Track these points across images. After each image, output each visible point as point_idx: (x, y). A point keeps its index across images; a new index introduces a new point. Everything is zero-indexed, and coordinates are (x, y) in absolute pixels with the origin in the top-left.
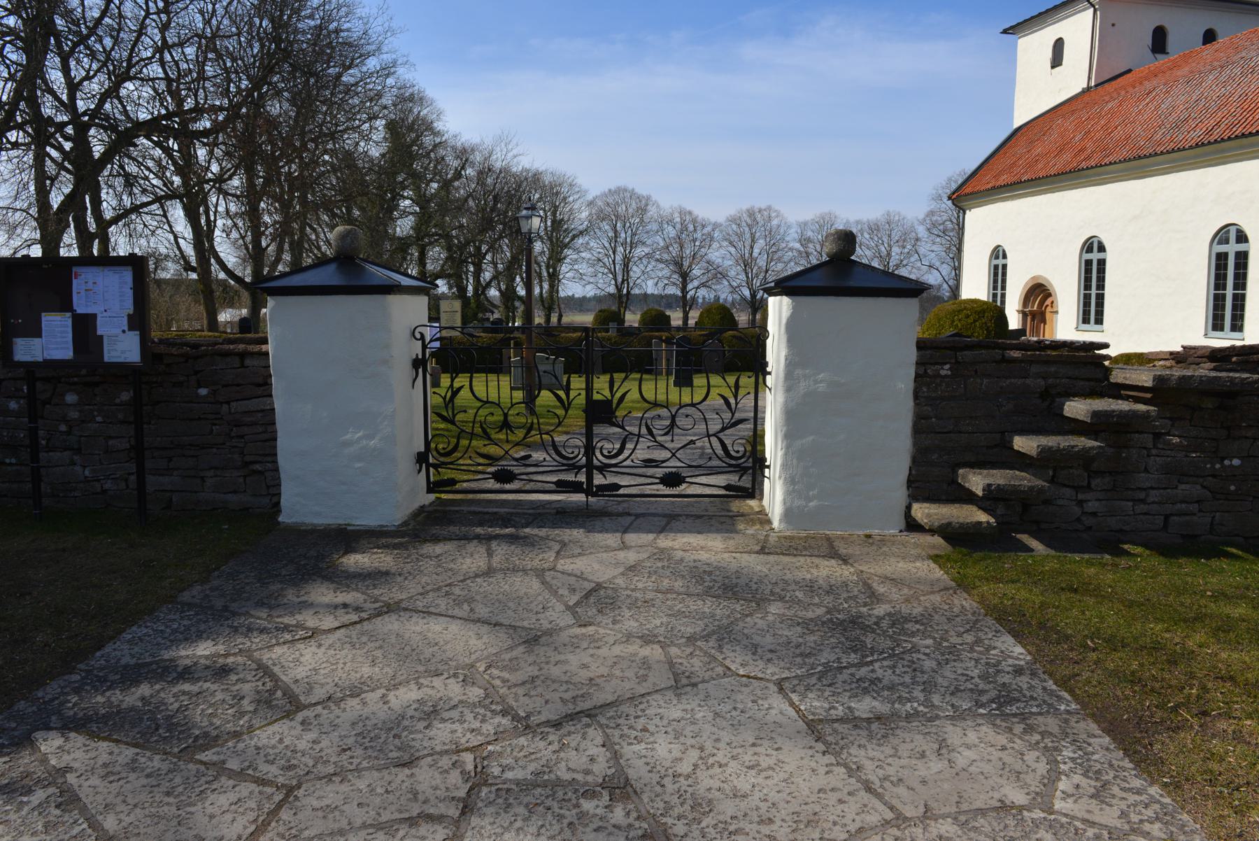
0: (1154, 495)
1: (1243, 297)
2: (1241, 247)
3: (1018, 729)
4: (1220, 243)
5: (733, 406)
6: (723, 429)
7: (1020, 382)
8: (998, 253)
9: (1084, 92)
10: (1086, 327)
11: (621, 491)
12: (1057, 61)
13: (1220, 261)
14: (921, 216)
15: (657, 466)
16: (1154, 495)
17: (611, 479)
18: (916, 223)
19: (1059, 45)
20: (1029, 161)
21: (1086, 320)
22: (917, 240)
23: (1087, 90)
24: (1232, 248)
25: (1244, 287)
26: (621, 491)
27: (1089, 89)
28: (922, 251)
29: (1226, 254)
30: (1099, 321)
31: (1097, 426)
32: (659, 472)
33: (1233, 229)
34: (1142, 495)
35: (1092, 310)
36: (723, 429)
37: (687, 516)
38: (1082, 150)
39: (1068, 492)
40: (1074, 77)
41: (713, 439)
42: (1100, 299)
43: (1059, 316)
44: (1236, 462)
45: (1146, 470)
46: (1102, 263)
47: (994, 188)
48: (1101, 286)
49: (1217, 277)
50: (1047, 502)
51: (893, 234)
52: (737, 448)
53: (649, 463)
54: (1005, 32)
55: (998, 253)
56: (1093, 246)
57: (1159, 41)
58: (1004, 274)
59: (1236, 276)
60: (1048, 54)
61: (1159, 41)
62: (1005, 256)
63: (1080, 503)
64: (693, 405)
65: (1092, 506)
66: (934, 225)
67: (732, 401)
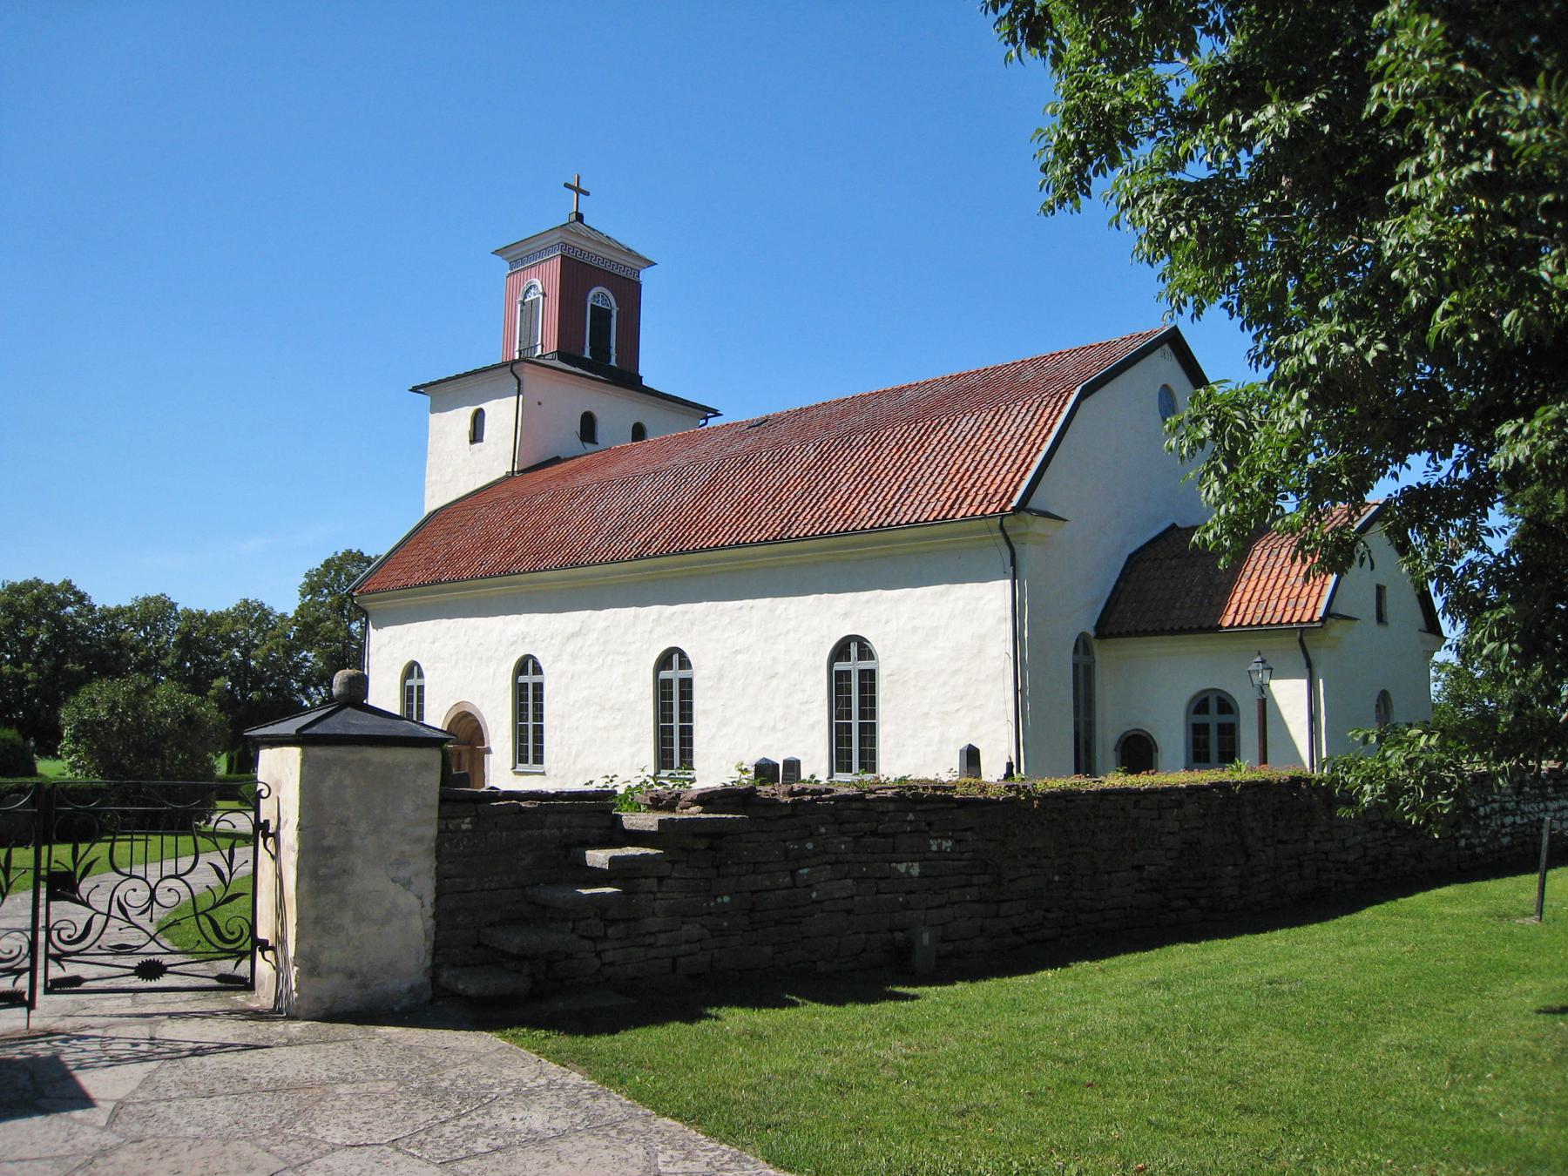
0: (663, 939)
1: (690, 729)
2: (866, 665)
3: (613, 1133)
5: (227, 877)
6: (216, 905)
7: (537, 833)
8: (412, 670)
10: (521, 767)
11: (86, 985)
12: (476, 435)
13: (838, 682)
15: (130, 953)
16: (663, 939)
17: (71, 970)
19: (478, 419)
20: (462, 559)
23: (510, 476)
25: (873, 714)
26: (86, 985)
30: (539, 759)
31: (618, 871)
32: (134, 961)
34: (651, 940)
35: (529, 747)
36: (216, 905)
37: (170, 1015)
38: (512, 550)
39: (587, 944)
40: (494, 459)
41: (202, 918)
42: (539, 731)
44: (726, 899)
45: (654, 914)
47: (405, 587)
48: (539, 716)
50: (569, 956)
52: (701, 845)
53: (121, 949)
54: (415, 389)
55: (412, 670)
56: (526, 665)
57: (588, 429)
58: (421, 699)
61: (588, 429)
62: (421, 675)
63: (598, 954)
64: (177, 876)
65: (609, 956)
67: (226, 871)
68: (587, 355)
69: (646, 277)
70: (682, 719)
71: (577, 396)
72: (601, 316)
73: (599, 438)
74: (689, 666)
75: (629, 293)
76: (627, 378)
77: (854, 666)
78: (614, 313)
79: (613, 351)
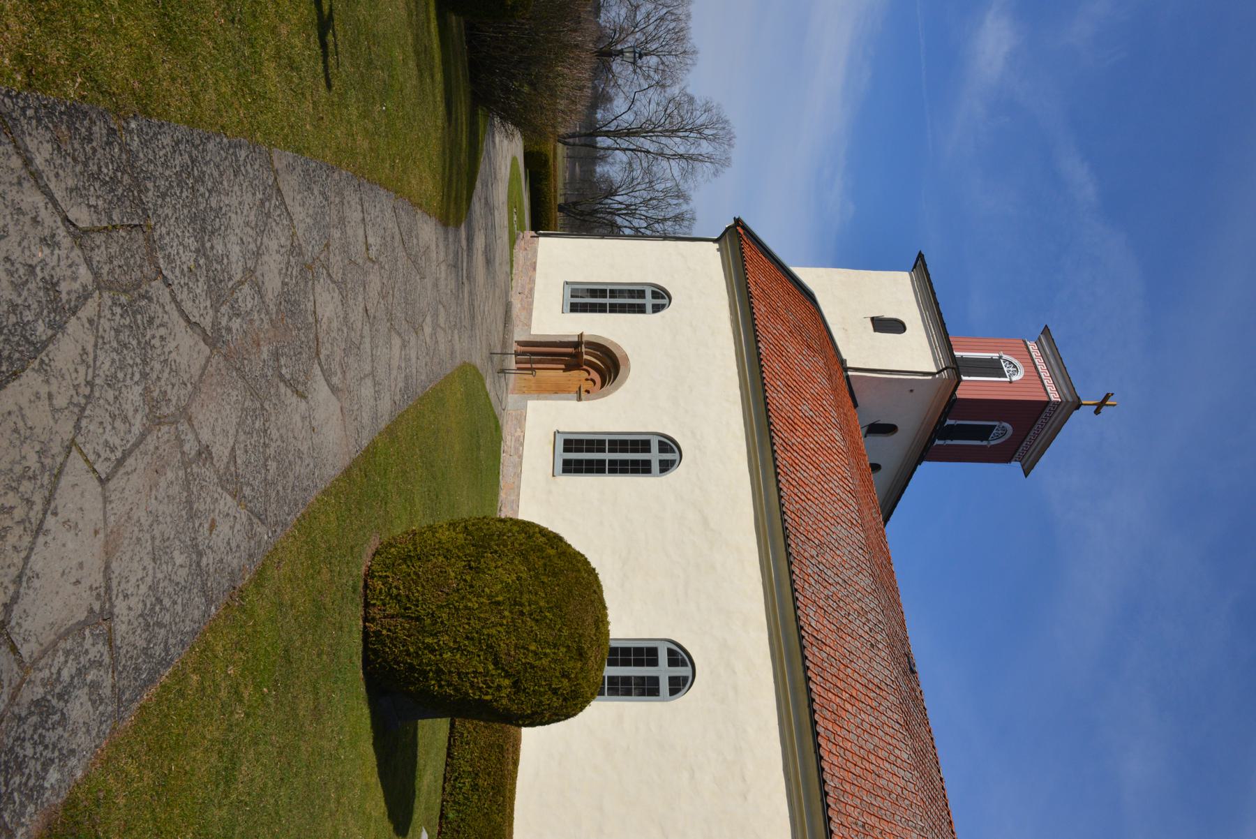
2: (655, 466)
4: (670, 652)
8: (661, 298)
9: (843, 362)
10: (560, 446)
13: (642, 445)
14: (689, 91)
18: (683, 84)
21: (567, 442)
22: (663, 86)
24: (655, 456)
25: (613, 471)
27: (847, 369)
28: (651, 91)
29: (649, 451)
30: (570, 467)
33: (675, 456)
40: (862, 350)
43: (574, 403)
46: (641, 309)
47: (750, 296)
48: (614, 309)
49: (624, 442)
51: (671, 58)
55: (661, 298)
57: (879, 429)
59: (624, 462)
60: (889, 314)
61: (879, 429)
66: (679, 106)
68: (949, 422)
69: (1016, 466)
70: (611, 305)
71: (910, 420)
72: (984, 433)
73: (871, 438)
74: (654, 312)
75: (1002, 455)
76: (926, 452)
77: (655, 456)
78: (985, 443)
79: (949, 442)
